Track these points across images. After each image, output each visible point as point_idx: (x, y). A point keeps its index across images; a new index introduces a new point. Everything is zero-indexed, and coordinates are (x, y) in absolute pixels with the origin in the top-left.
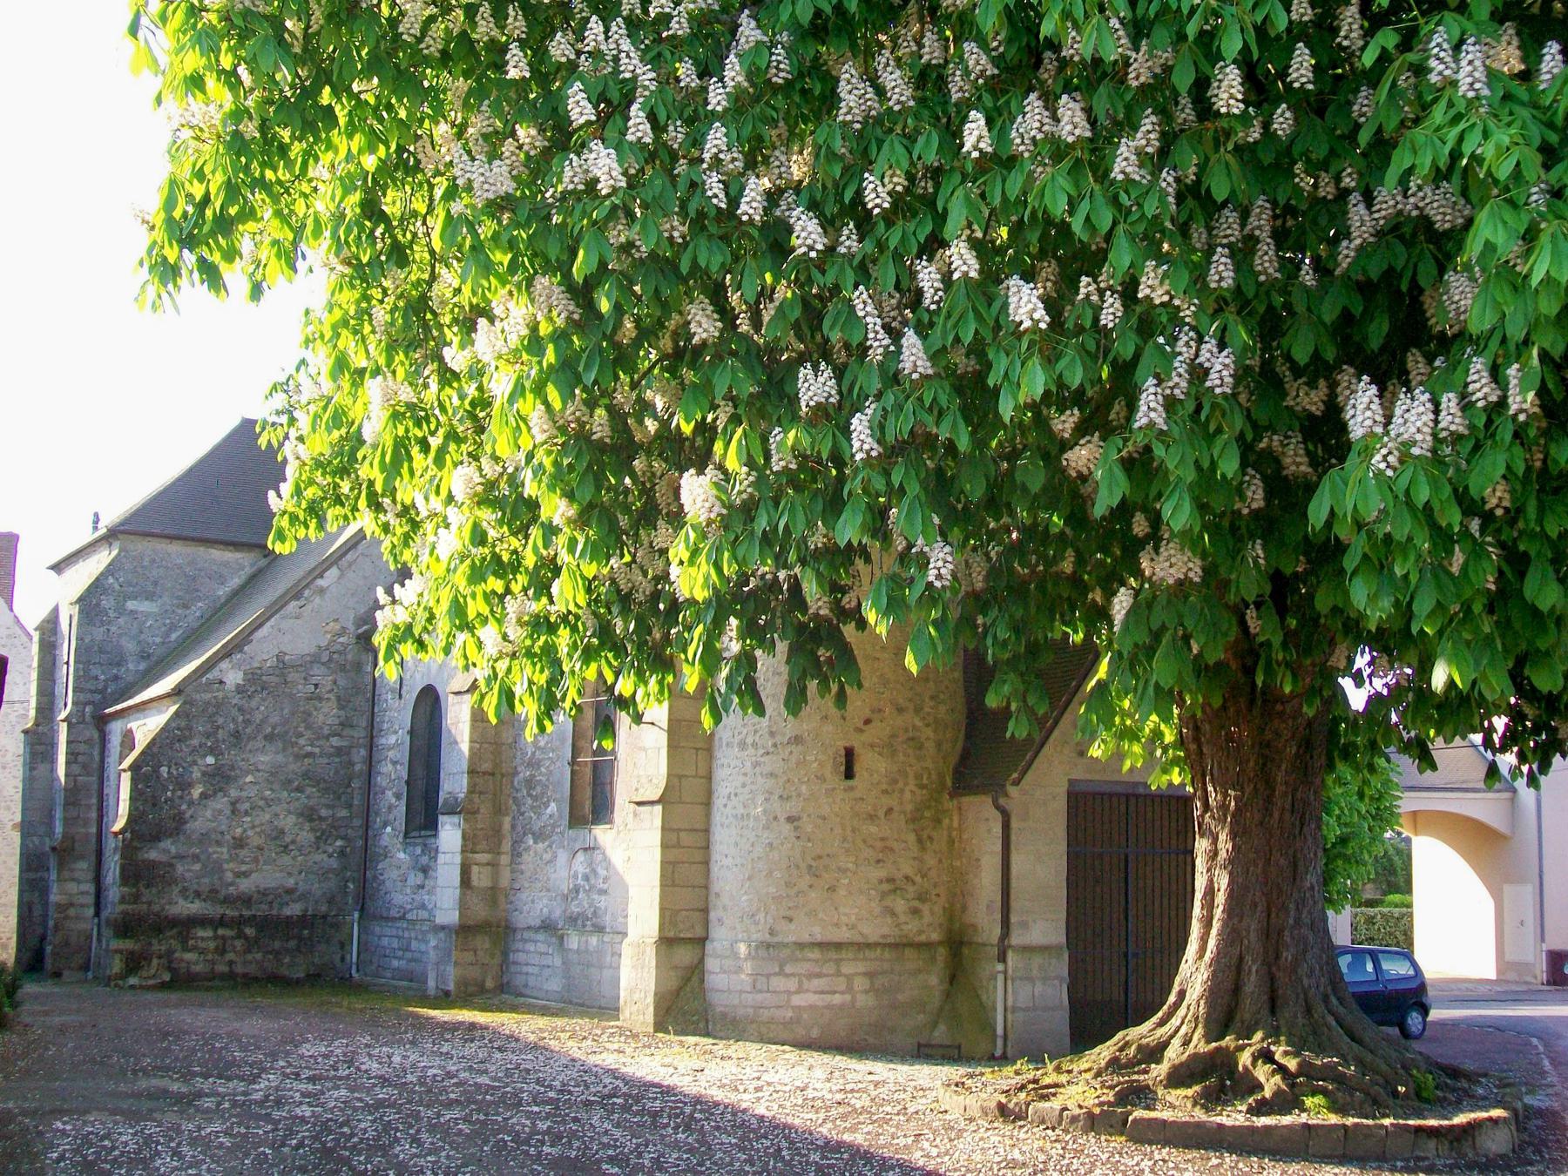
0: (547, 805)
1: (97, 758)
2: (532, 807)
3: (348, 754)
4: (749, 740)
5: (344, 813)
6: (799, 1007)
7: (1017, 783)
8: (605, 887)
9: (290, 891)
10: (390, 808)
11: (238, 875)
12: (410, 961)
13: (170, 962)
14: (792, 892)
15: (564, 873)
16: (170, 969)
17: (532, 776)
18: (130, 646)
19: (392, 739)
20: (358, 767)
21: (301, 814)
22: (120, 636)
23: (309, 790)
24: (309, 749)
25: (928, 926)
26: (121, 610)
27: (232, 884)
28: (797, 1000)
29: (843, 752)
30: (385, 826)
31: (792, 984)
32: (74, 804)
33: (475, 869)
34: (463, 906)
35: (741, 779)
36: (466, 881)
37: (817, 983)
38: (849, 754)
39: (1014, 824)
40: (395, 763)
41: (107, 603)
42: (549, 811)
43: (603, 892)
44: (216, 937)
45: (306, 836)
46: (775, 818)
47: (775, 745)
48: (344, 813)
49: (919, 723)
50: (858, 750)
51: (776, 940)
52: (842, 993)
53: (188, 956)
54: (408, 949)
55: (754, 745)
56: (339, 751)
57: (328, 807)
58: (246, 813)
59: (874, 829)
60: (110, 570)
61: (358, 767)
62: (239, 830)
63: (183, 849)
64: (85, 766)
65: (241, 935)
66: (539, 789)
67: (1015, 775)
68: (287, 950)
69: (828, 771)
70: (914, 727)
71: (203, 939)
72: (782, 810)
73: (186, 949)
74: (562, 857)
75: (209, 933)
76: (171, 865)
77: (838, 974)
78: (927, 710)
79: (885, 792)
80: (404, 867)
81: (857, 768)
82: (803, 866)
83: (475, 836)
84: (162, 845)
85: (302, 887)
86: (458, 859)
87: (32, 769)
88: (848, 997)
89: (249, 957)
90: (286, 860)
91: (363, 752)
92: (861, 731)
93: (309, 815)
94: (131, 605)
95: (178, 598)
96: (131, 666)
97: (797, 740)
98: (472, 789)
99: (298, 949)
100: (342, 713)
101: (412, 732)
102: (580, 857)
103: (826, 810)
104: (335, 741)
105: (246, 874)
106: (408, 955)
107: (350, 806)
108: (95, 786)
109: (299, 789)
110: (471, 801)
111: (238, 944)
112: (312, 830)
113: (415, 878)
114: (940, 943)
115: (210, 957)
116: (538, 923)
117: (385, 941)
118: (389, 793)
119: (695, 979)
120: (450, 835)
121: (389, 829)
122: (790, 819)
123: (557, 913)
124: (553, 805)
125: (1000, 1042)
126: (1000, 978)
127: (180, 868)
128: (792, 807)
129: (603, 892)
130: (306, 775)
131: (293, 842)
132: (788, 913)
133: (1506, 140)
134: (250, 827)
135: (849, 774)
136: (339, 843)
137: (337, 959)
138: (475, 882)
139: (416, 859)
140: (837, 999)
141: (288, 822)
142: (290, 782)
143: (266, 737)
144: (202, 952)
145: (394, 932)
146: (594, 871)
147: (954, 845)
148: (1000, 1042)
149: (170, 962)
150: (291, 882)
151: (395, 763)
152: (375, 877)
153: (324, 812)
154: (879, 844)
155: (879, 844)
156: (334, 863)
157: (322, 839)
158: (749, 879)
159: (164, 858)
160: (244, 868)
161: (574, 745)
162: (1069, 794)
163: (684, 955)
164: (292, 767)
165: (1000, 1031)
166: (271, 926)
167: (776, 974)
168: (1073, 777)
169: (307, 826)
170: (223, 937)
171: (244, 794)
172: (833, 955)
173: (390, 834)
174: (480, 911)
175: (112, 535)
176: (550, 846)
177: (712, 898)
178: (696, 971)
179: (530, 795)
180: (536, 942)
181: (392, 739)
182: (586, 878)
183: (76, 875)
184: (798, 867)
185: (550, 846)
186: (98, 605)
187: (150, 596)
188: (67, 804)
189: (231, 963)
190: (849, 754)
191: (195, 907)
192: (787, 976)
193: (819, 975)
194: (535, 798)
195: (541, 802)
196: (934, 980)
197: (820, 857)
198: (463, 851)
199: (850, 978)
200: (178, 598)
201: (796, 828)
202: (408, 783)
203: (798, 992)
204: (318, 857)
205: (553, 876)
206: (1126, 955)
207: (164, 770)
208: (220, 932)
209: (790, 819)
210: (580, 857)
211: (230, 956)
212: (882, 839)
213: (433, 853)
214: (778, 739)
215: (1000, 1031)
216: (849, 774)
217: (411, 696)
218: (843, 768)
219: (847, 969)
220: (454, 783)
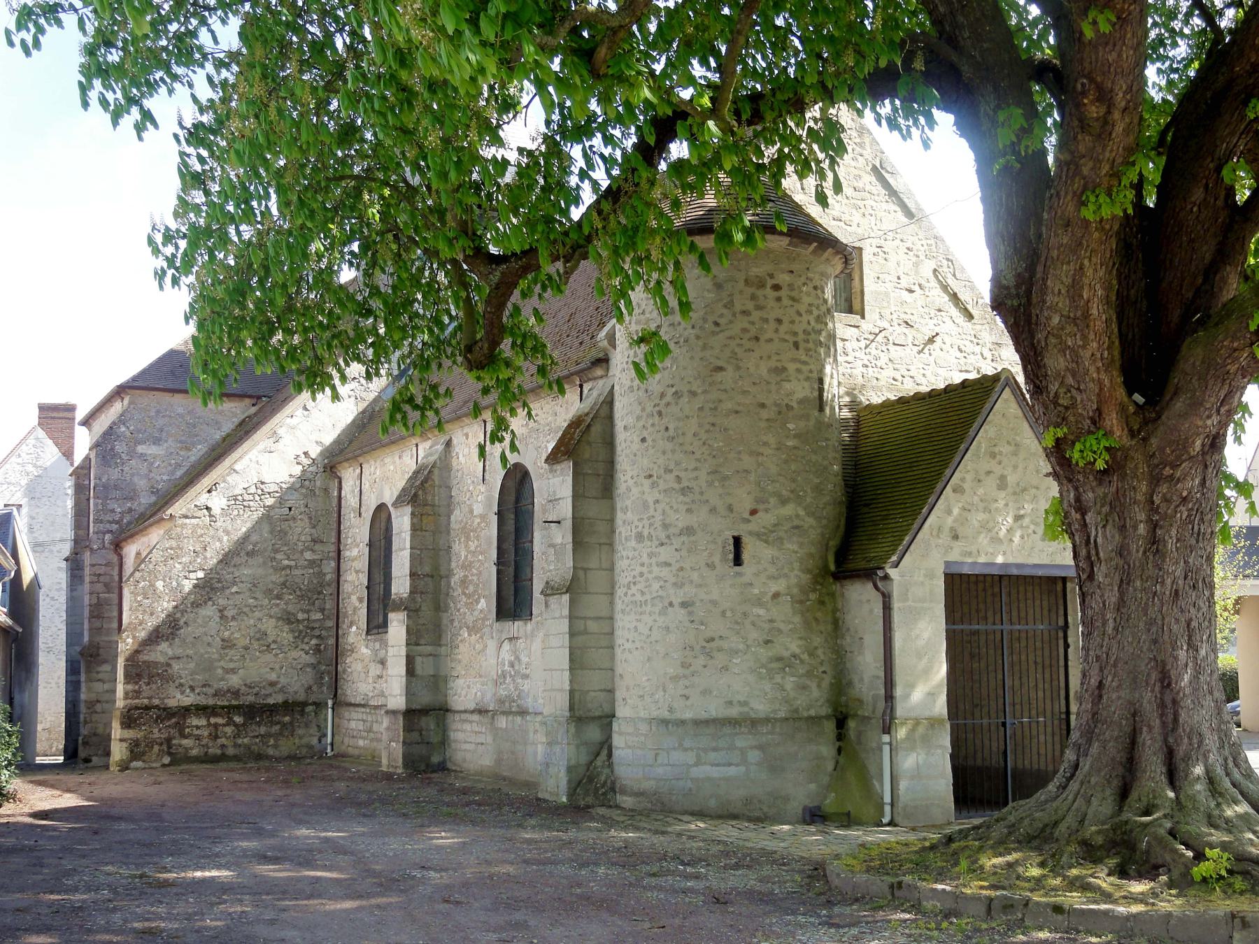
0: (478, 602)
1: (117, 578)
2: (466, 604)
3: (320, 566)
4: (646, 534)
5: (319, 616)
6: (697, 780)
7: (896, 565)
8: (528, 672)
9: (272, 684)
10: (355, 609)
11: (227, 671)
12: (372, 740)
13: (169, 747)
14: (687, 672)
15: (493, 661)
16: (170, 754)
17: (466, 576)
18: (141, 483)
19: (355, 552)
20: (328, 577)
21: (279, 619)
22: (133, 475)
23: (287, 597)
24: (286, 562)
25: (815, 699)
26: (132, 453)
27: (222, 679)
28: (697, 772)
29: (731, 541)
30: (351, 627)
31: (690, 758)
32: (98, 617)
33: (418, 660)
34: (409, 693)
35: (639, 569)
36: (410, 671)
37: (712, 756)
38: (737, 541)
39: (896, 605)
40: (357, 572)
41: (120, 448)
42: (479, 606)
43: (526, 677)
44: (209, 724)
45: (286, 636)
46: (671, 604)
47: (668, 537)
48: (319, 616)
49: (802, 513)
50: (746, 540)
51: (673, 717)
52: (737, 765)
53: (185, 742)
54: (370, 731)
55: (650, 537)
56: (312, 563)
57: (304, 611)
58: (233, 618)
59: (761, 612)
60: (122, 419)
61: (328, 577)
62: (227, 633)
63: (179, 652)
64: (106, 585)
65: (230, 722)
66: (471, 588)
67: (894, 558)
68: (270, 735)
69: (717, 559)
70: (797, 516)
71: (198, 727)
72: (677, 597)
73: (183, 736)
74: (492, 645)
75: (203, 722)
76: (169, 665)
77: (732, 748)
78: (809, 500)
79: (772, 578)
80: (367, 660)
81: (745, 556)
82: (697, 648)
83: (418, 631)
84: (159, 648)
85: (283, 681)
86: (403, 651)
87: (72, 590)
88: (743, 769)
89: (239, 741)
90: (269, 657)
91: (333, 564)
92: (749, 521)
93: (288, 619)
94: (140, 449)
95: (181, 442)
96: (143, 501)
97: (689, 531)
98: (413, 591)
99: (281, 734)
100: (313, 531)
101: (370, 545)
102: (506, 646)
103: (715, 595)
104: (308, 555)
105: (233, 671)
106: (372, 735)
107: (322, 610)
108: (116, 601)
109: (279, 597)
110: (414, 600)
111: (229, 730)
112: (292, 631)
113: (375, 670)
114: (827, 717)
115: (205, 741)
116: (472, 706)
117: (353, 725)
118: (354, 598)
119: (605, 752)
120: (397, 627)
121: (354, 628)
122: (684, 605)
123: (489, 696)
124: (482, 600)
125: (887, 809)
126: (886, 749)
127: (176, 666)
128: (689, 591)
129: (526, 677)
130: (284, 584)
131: (274, 642)
132: (686, 692)
133: (1224, 24)
134: (239, 633)
135: (738, 561)
136: (314, 642)
137: (315, 741)
138: (419, 670)
139: (375, 652)
140: (732, 771)
141: (269, 625)
142: (271, 591)
143: (247, 554)
144: (198, 738)
145: (360, 716)
146: (517, 658)
147: (837, 626)
148: (887, 809)
149: (169, 747)
150: (273, 677)
151: (357, 572)
152: (344, 671)
153: (300, 616)
154: (767, 626)
155: (767, 626)
156: (309, 659)
157: (300, 637)
158: (649, 659)
159: (161, 659)
160: (232, 665)
161: (499, 548)
162: (946, 575)
163: (593, 733)
164: (274, 578)
165: (887, 799)
166: (255, 712)
167: (674, 749)
168: (951, 558)
169: (286, 628)
170: (216, 726)
171: (231, 602)
172: (727, 730)
173: (355, 633)
174: (425, 699)
175: (120, 391)
176: (481, 638)
177: (617, 679)
178: (605, 746)
179: (464, 593)
180: (471, 722)
181: (355, 552)
182: (512, 665)
183: (100, 676)
184: (692, 648)
185: (481, 638)
186: (112, 449)
187: (157, 441)
188: (92, 617)
189: (223, 746)
190: (737, 541)
191: (188, 699)
192: (686, 750)
193: (715, 749)
194: (468, 596)
195: (473, 599)
196: (827, 750)
197: (713, 639)
198: (407, 644)
199: (743, 752)
200: (181, 442)
201: (690, 613)
202: (368, 588)
203: (696, 765)
204: (295, 654)
205: (484, 664)
206: (1004, 724)
207: (160, 584)
208: (213, 720)
209: (684, 605)
210: (506, 646)
211: (223, 741)
212: (771, 621)
213: (385, 644)
214: (672, 530)
215: (887, 799)
216: (738, 561)
217: (368, 515)
218: (731, 556)
219: (740, 743)
220: (401, 585)
